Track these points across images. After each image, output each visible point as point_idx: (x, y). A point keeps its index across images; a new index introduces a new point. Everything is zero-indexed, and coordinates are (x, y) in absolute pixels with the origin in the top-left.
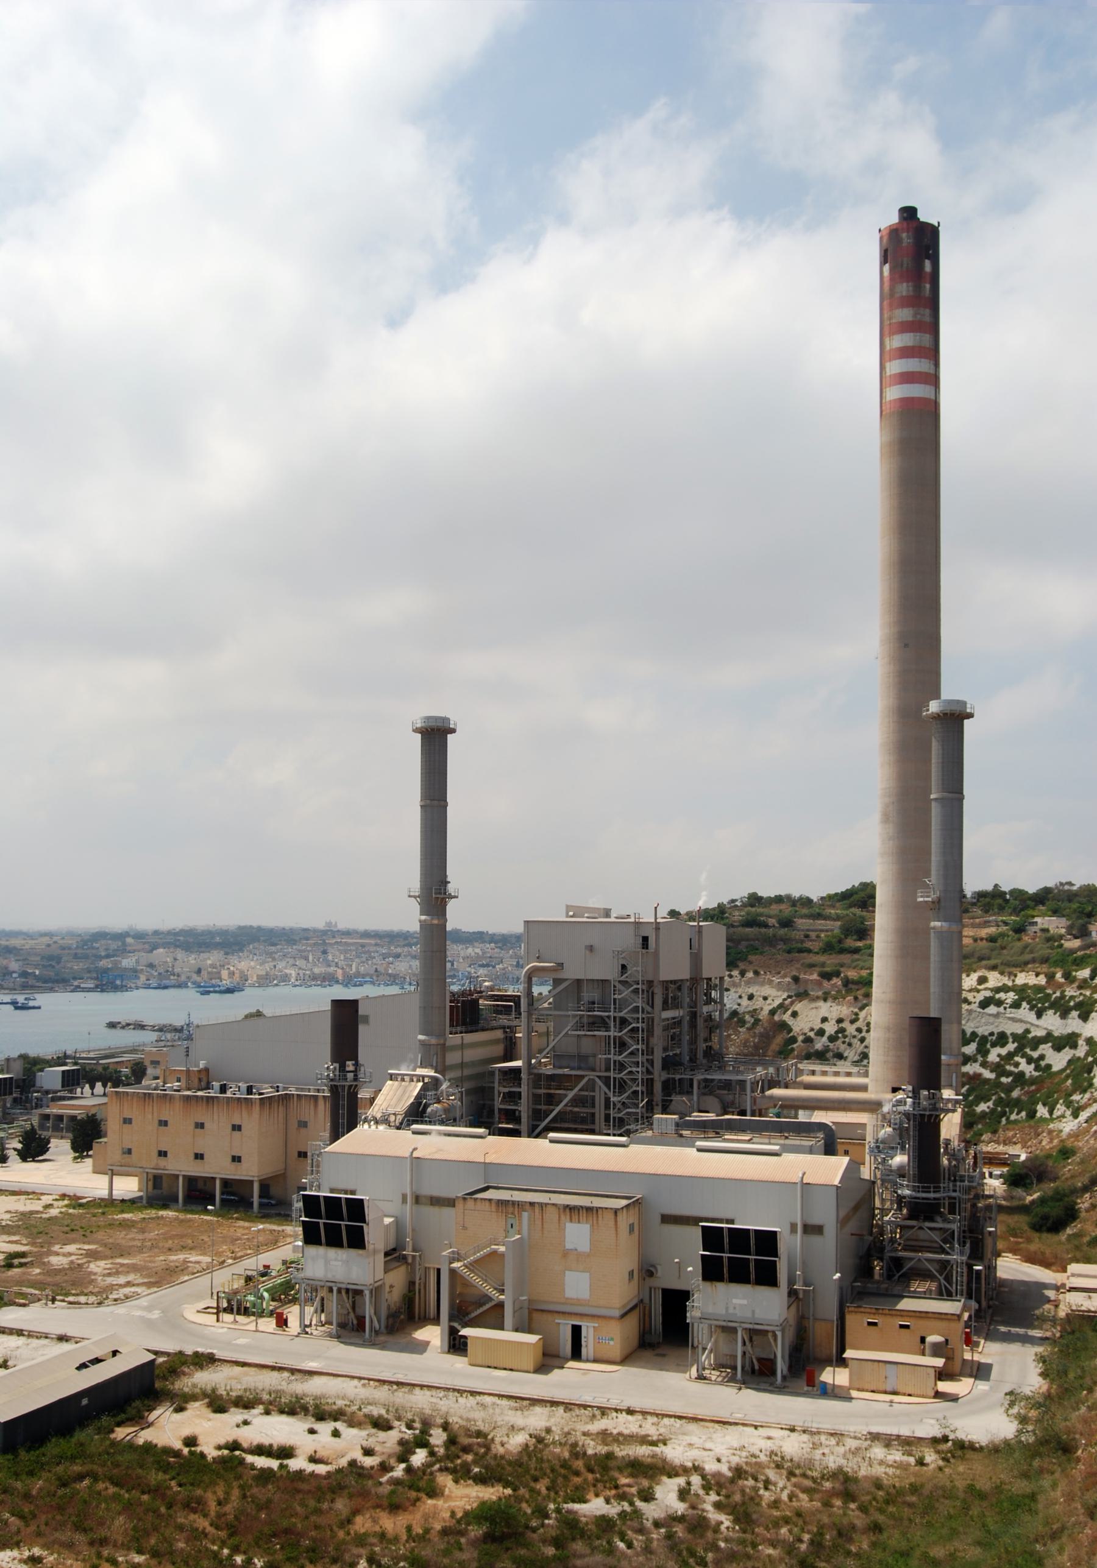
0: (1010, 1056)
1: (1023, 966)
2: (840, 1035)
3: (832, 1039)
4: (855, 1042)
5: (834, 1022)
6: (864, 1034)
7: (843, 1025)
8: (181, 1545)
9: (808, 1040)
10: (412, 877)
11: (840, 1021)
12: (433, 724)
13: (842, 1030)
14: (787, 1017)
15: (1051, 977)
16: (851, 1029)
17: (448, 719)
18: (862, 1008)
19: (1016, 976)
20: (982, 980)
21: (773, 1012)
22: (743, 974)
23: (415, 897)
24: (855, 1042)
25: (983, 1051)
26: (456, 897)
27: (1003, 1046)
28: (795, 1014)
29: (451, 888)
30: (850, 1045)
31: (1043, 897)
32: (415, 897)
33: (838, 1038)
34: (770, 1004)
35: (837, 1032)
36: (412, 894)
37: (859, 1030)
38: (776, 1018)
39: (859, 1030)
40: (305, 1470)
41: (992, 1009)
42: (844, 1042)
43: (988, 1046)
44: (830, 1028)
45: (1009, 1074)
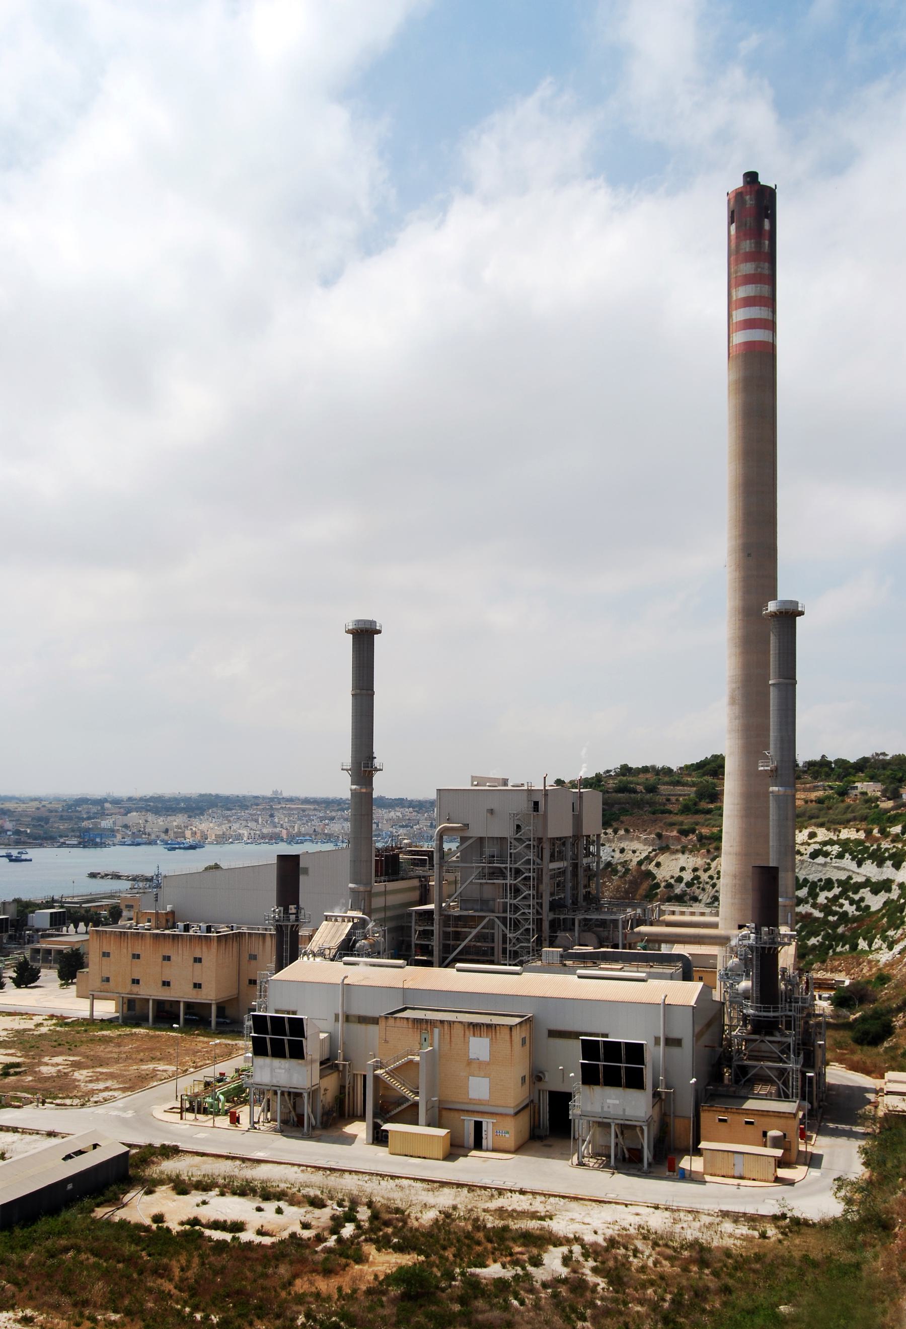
0: (836, 898)
1: (846, 823)
2: (695, 882)
3: (689, 885)
4: (708, 887)
7: (698, 873)
9: (669, 886)
10: (345, 754)
11: (695, 870)
12: (362, 626)
13: (697, 878)
14: (651, 867)
15: (869, 833)
16: (704, 877)
17: (375, 622)
18: (713, 860)
19: (840, 832)
21: (640, 863)
23: (347, 770)
24: (708, 887)
25: (813, 894)
27: (830, 890)
28: (658, 865)
29: (377, 763)
32: (347, 770)
35: (692, 879)
36: (344, 768)
37: (711, 877)
38: (643, 868)
39: (711, 877)
40: (253, 1242)
42: (699, 888)
45: (834, 913)
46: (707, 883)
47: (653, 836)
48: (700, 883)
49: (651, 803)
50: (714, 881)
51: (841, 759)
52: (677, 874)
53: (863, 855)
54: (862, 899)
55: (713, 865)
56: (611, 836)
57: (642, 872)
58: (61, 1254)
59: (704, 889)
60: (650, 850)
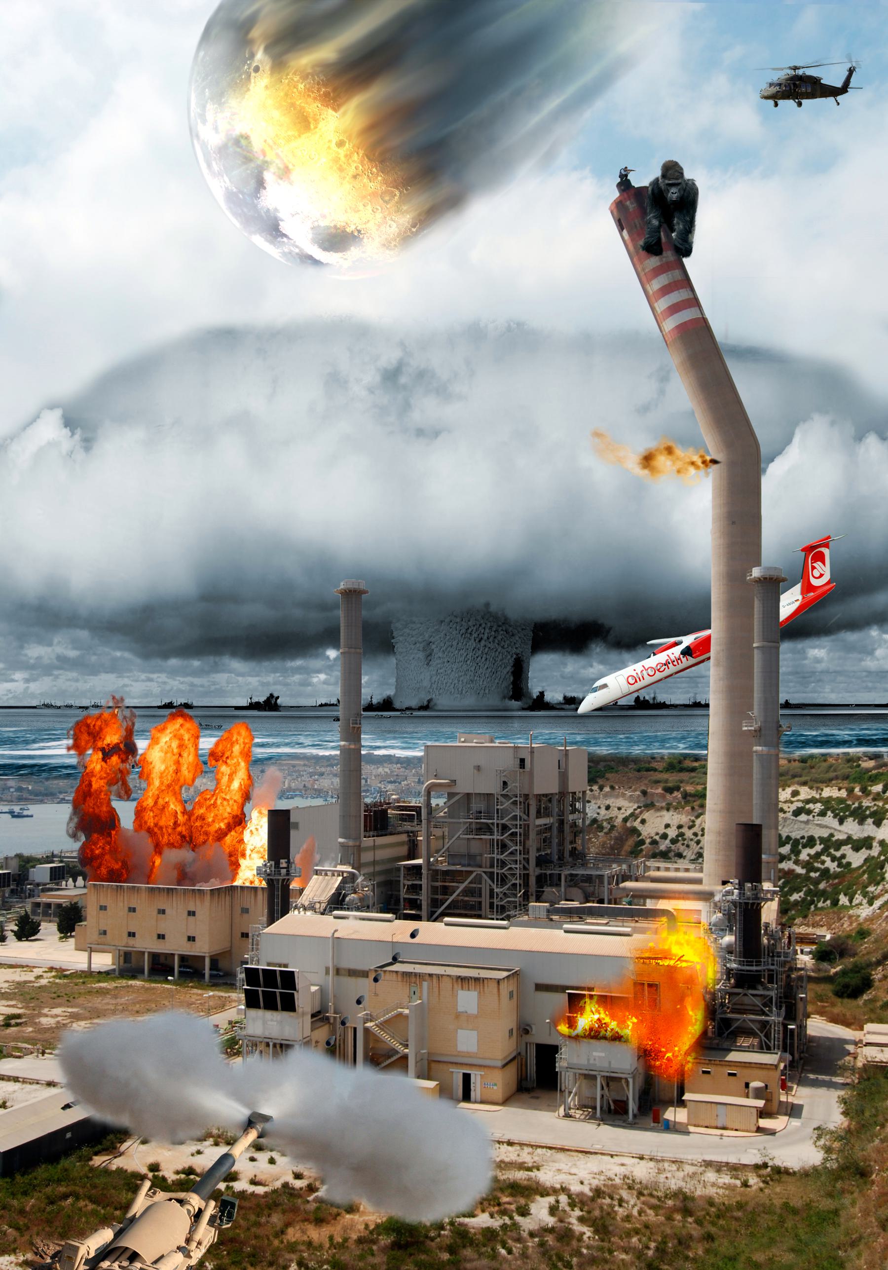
0: (818, 855)
1: (828, 782)
2: (680, 838)
3: (674, 841)
4: (692, 844)
5: (675, 828)
6: (699, 837)
9: (654, 842)
13: (682, 835)
14: (637, 824)
15: (850, 791)
16: (689, 834)
18: (697, 817)
19: (822, 790)
24: (692, 844)
25: (796, 851)
28: (643, 822)
35: (677, 836)
37: (695, 834)
38: (628, 824)
41: (803, 817)
42: (683, 844)
43: (800, 847)
44: (672, 833)
45: (816, 870)
47: (638, 793)
52: (662, 831)
55: (698, 822)
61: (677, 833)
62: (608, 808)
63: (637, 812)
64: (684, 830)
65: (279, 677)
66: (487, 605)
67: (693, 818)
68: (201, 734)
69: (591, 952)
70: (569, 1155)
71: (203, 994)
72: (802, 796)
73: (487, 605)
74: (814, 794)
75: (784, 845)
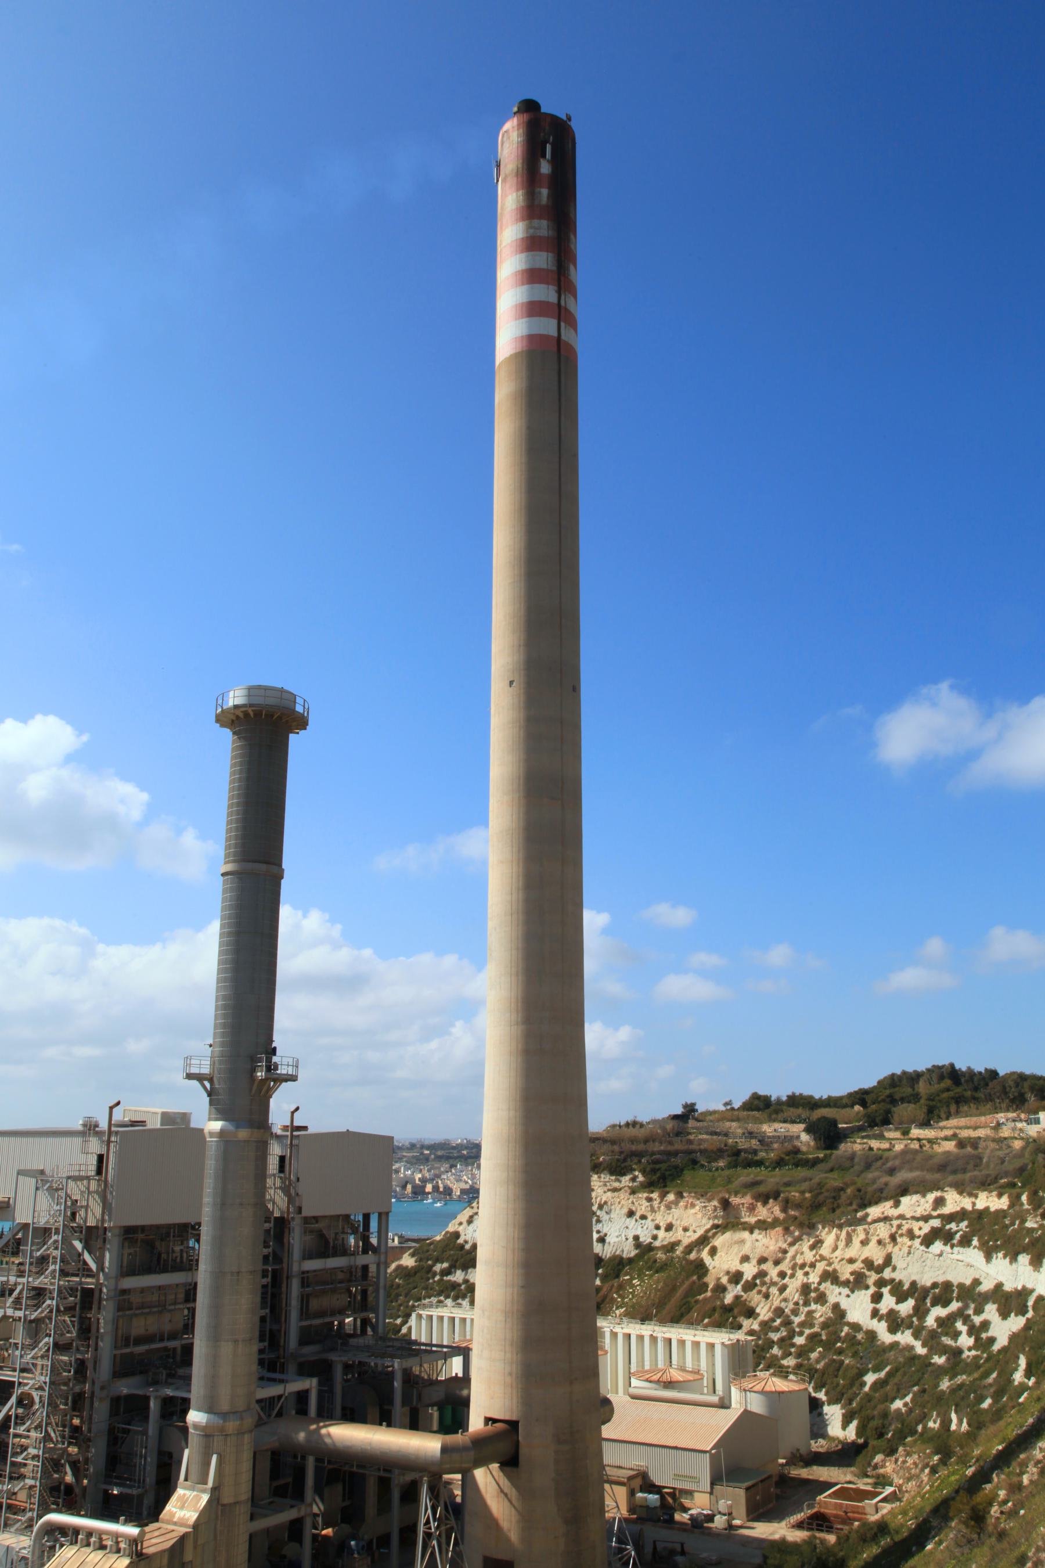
0: (951, 1318)
1: (985, 1184)
2: (758, 1281)
3: (749, 1286)
4: (774, 1291)
5: (754, 1262)
6: (787, 1280)
7: (764, 1267)
8: (772, 1155)
9: (721, 1289)
11: (762, 1260)
15: (1015, 1201)
16: (773, 1273)
18: (792, 1244)
19: (976, 1197)
20: (939, 1202)
21: (689, 1249)
22: (663, 1196)
23: (199, 1078)
24: (774, 1291)
25: (920, 1312)
26: (293, 1078)
27: (946, 1304)
28: (713, 1252)
30: (767, 1296)
31: (798, 1123)
32: (199, 1078)
33: (756, 1285)
34: (689, 1237)
35: (755, 1277)
36: (194, 1070)
37: (782, 1275)
38: (693, 1256)
39: (782, 1275)
41: (938, 1246)
42: (759, 1292)
43: (928, 1301)
44: (749, 1271)
45: (944, 1350)
46: (774, 1284)
47: (715, 1203)
48: (763, 1283)
49: (954, 1172)
50: (785, 1281)
51: (1014, 1073)
52: (735, 1265)
53: (617, 1298)
54: (986, 1325)
55: (792, 1251)
56: (656, 1204)
57: (692, 1262)
58: (861, 1389)
59: (767, 1296)
60: (708, 1226)
61: (755, 1271)
62: (669, 1228)
63: (710, 1234)
64: (767, 1266)
65: (434, 1202)
66: (504, 1247)
67: (785, 1246)
68: (626, 1480)
69: (627, 1502)
70: (486, 1473)
71: (755, 1176)
72: (948, 1209)
73: (504, 1247)
74: (966, 1203)
75: (906, 1299)
